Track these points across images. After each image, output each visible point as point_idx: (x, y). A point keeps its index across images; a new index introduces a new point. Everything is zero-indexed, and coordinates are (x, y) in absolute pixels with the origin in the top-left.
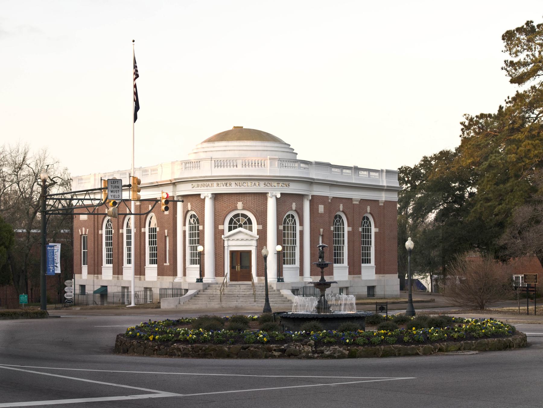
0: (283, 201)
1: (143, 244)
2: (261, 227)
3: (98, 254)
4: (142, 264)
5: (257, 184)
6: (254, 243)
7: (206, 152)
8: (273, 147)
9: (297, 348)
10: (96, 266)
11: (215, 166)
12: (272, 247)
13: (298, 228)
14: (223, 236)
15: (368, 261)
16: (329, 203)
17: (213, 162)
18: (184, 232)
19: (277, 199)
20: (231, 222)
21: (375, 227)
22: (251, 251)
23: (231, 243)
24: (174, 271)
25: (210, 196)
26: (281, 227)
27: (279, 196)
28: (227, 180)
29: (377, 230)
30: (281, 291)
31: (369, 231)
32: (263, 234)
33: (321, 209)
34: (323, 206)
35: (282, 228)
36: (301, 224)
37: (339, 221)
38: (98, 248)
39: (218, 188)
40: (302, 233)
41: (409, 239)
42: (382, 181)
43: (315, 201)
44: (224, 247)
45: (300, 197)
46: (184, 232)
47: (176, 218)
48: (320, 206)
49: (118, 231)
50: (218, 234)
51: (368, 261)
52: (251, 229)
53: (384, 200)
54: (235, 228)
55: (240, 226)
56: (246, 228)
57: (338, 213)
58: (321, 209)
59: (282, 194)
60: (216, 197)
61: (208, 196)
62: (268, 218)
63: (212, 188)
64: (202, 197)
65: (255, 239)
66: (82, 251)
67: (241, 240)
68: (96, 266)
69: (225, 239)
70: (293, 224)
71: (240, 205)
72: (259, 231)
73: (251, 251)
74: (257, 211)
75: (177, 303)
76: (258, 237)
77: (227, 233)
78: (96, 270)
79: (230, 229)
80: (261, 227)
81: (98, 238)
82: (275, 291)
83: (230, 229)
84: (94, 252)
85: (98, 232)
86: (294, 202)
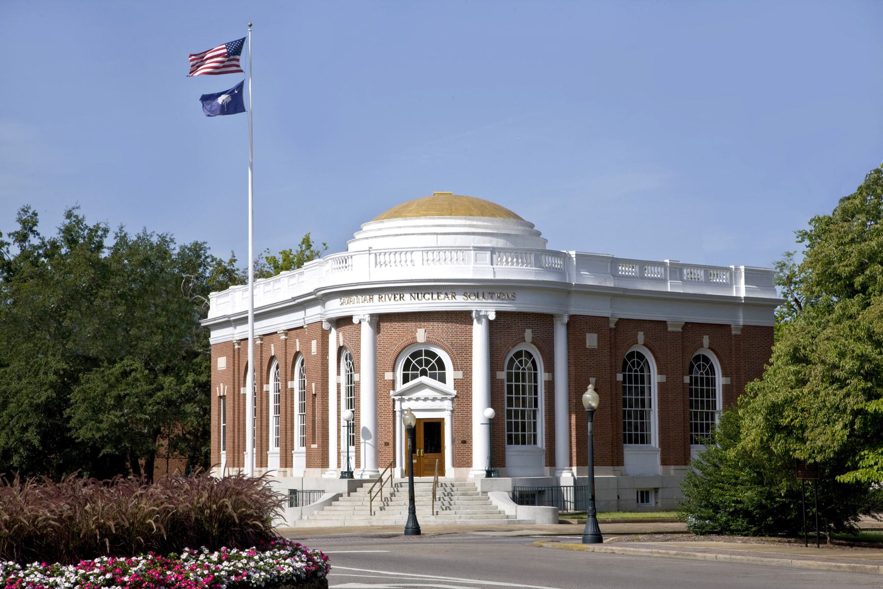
0: (499, 328)
1: (289, 409)
2: (460, 375)
3: (239, 429)
4: (289, 447)
5: (398, 296)
6: (447, 405)
7: (367, 238)
8: (465, 226)
9: (126, 579)
10: (236, 451)
11: (376, 264)
12: (481, 412)
13: (542, 376)
14: (392, 392)
15: (643, 439)
16: (611, 330)
17: (373, 256)
18: (339, 385)
19: (490, 323)
20: (407, 367)
21: (660, 372)
22: (443, 419)
23: (406, 405)
24: (323, 459)
25: (368, 318)
26: (502, 375)
27: (492, 316)
28: (397, 290)
29: (728, 381)
30: (489, 494)
31: (711, 382)
32: (464, 386)
33: (592, 340)
34: (595, 336)
35: (688, 381)
36: (550, 367)
37: (639, 364)
38: (239, 419)
39: (381, 303)
40: (550, 386)
41: (591, 387)
42: (738, 289)
43: (576, 325)
44: (394, 412)
45: (464, 317)
46: (339, 385)
47: (327, 360)
48: (588, 335)
49: (262, 388)
50: (381, 388)
51: (643, 439)
52: (443, 379)
53: (741, 323)
54: (415, 377)
55: (423, 373)
56: (433, 376)
57: (701, 352)
58: (592, 340)
59: (498, 313)
60: (379, 320)
61: (364, 320)
62: (474, 358)
63: (371, 304)
64: (355, 321)
65: (449, 397)
66: (222, 425)
67: (428, 401)
68: (236, 451)
69: (396, 398)
70: (707, 373)
71: (528, 334)
72: (457, 383)
73: (443, 419)
74: (452, 344)
75: (297, 517)
76: (455, 393)
77: (400, 387)
78: (236, 462)
79: (406, 379)
80: (460, 375)
81: (239, 399)
82: (478, 494)
83: (406, 379)
84: (234, 427)
85: (239, 390)
86: (529, 328)
